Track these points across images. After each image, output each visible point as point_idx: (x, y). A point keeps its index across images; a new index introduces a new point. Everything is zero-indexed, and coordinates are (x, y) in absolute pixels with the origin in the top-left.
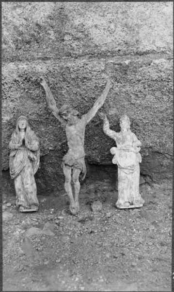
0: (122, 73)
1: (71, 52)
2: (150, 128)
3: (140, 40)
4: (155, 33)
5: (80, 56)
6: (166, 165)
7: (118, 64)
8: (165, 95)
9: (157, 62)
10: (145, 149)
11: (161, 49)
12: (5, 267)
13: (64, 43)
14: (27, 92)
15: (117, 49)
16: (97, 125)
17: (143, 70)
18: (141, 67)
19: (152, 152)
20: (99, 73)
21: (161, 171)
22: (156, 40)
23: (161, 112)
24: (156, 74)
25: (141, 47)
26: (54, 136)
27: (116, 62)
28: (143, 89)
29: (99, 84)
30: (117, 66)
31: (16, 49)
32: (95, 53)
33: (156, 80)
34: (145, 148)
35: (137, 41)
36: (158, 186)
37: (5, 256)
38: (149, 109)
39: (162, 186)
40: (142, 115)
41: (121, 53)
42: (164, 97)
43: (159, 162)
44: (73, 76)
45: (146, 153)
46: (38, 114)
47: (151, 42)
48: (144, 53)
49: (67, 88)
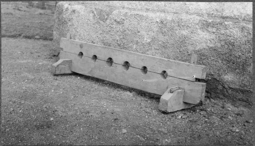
0: (206, 26)
1: (188, 11)
2: (215, 63)
3: (224, 9)
4: (234, 6)
5: (193, 14)
6: (220, 89)
7: (206, 21)
8: (227, 44)
9: (226, 23)
10: (209, 75)
11: (237, 17)
12: (73, 3)
13: (186, 6)
14: (161, 29)
15: (211, 13)
16: (189, 55)
17: (217, 26)
18: (217, 25)
19: (213, 78)
20: (195, 25)
21: (216, 92)
22: (234, 11)
23: (223, 55)
24: (224, 30)
25: (224, 13)
26: (167, 56)
27: (205, 20)
28: (215, 39)
29: (194, 31)
30: (205, 22)
31: (165, 6)
32: (200, 13)
33: (223, 34)
34: (209, 74)
35: (223, 9)
36: (213, 101)
37: (73, 3)
38: (216, 51)
39: (216, 102)
40: (211, 54)
41: (213, 15)
42: (226, 45)
43: (216, 86)
44: (183, 24)
45: (209, 78)
46: (163, 41)
47: (231, 11)
48: (225, 17)
49: (179, 31)
